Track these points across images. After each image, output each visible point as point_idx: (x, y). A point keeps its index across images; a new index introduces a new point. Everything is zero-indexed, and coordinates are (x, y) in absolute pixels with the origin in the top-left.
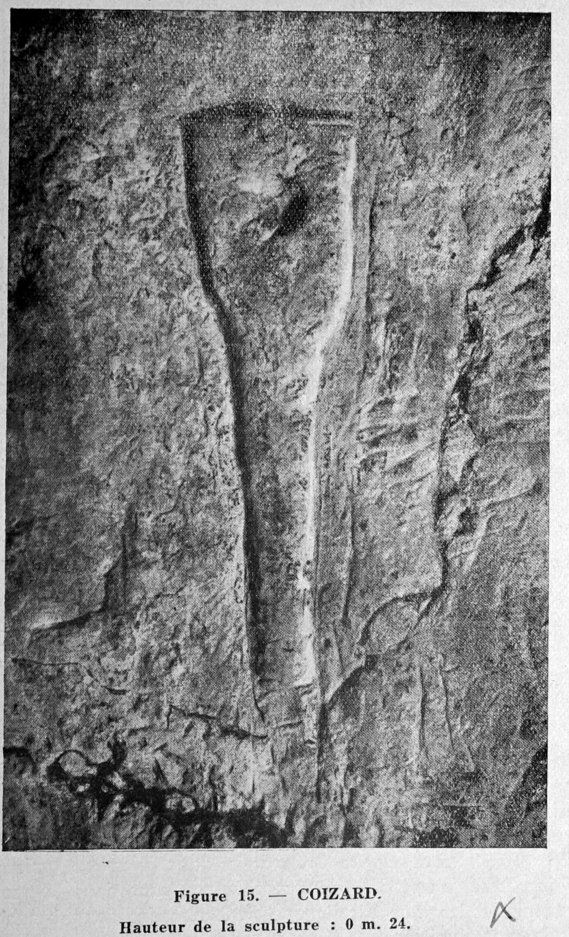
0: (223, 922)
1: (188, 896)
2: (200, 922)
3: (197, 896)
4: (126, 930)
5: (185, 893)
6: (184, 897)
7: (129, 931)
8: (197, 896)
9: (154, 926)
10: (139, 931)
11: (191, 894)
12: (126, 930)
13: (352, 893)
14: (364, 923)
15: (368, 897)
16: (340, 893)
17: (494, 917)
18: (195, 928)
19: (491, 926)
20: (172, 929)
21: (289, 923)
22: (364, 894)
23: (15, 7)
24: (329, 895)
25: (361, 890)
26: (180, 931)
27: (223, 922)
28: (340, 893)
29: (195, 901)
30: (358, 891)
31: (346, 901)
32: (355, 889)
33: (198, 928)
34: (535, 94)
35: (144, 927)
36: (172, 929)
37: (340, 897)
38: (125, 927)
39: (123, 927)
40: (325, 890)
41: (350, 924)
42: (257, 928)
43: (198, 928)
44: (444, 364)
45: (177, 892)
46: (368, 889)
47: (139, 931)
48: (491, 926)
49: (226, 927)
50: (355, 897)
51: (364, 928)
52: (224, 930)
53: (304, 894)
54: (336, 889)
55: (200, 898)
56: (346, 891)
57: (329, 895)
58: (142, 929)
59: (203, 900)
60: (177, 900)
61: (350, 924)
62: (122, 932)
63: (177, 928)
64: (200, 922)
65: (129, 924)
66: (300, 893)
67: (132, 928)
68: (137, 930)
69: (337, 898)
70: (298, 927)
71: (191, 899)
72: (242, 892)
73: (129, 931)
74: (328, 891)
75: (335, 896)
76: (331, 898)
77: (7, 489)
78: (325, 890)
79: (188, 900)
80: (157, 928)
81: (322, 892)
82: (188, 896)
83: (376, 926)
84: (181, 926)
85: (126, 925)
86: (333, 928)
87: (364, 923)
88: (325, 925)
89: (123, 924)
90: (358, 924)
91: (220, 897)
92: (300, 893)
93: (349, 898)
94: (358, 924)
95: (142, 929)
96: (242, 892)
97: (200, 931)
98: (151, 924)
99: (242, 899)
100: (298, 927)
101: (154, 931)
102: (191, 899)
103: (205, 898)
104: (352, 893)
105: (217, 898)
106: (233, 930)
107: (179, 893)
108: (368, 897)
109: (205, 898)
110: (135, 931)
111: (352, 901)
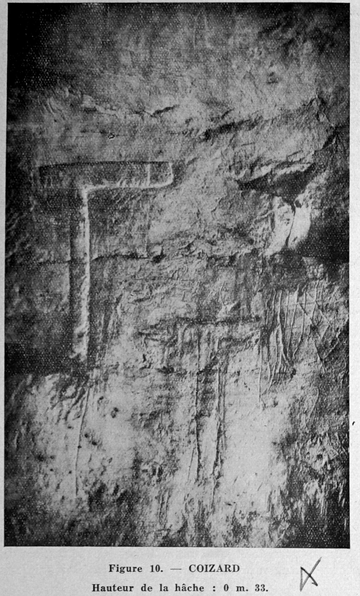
0: (161, 585)
1: (118, 568)
2: (145, 585)
3: (124, 568)
4: (96, 589)
5: (116, 566)
6: (115, 569)
7: (98, 590)
8: (124, 568)
9: (114, 586)
10: (104, 591)
11: (119, 567)
12: (96, 589)
13: (224, 569)
14: (238, 587)
15: (234, 571)
16: (216, 568)
17: (301, 583)
18: (142, 588)
19: (301, 589)
20: (125, 589)
21: (114, 586)
22: (231, 569)
23: (3, 544)
24: (209, 569)
25: (230, 566)
26: (131, 590)
27: (161, 585)
28: (216, 568)
29: (122, 572)
30: (228, 567)
31: (220, 573)
32: (226, 566)
33: (144, 588)
34: (304, 136)
35: (108, 587)
36: (125, 589)
37: (216, 570)
38: (95, 588)
39: (94, 588)
40: (206, 566)
41: (226, 588)
42: (190, 589)
43: (144, 588)
44: (234, 302)
45: (111, 566)
46: (234, 566)
47: (104, 591)
48: (301, 589)
49: (163, 589)
50: (226, 571)
51: (238, 590)
52: (161, 590)
53: (193, 568)
54: (214, 565)
55: (125, 570)
56: (220, 567)
57: (209, 569)
58: (106, 589)
59: (128, 571)
60: (111, 571)
61: (226, 588)
62: (94, 590)
63: (129, 589)
64: (145, 585)
65: (98, 585)
66: (190, 567)
67: (100, 589)
68: (103, 589)
69: (214, 571)
70: (109, 589)
71: (119, 570)
72: (152, 566)
73: (98, 590)
74: (208, 567)
75: (213, 570)
76: (210, 571)
77: (10, 95)
78: (206, 566)
79: (118, 571)
80: (116, 588)
81: (205, 567)
82: (118, 568)
83: (245, 589)
84: (131, 587)
85: (96, 586)
86: (214, 590)
87: (238, 587)
88: (208, 589)
89: (94, 585)
90: (232, 588)
91: (138, 569)
92: (190, 567)
93: (222, 571)
94: (172, 588)
95: (106, 589)
96: (152, 566)
97: (145, 590)
98: (112, 586)
99: (152, 571)
100: (109, 589)
101: (114, 590)
102: (119, 570)
103: (129, 570)
104: (224, 569)
105: (136, 570)
106: (167, 590)
107: (112, 566)
108: (234, 571)
109: (129, 570)
110: (101, 590)
111: (224, 573)
